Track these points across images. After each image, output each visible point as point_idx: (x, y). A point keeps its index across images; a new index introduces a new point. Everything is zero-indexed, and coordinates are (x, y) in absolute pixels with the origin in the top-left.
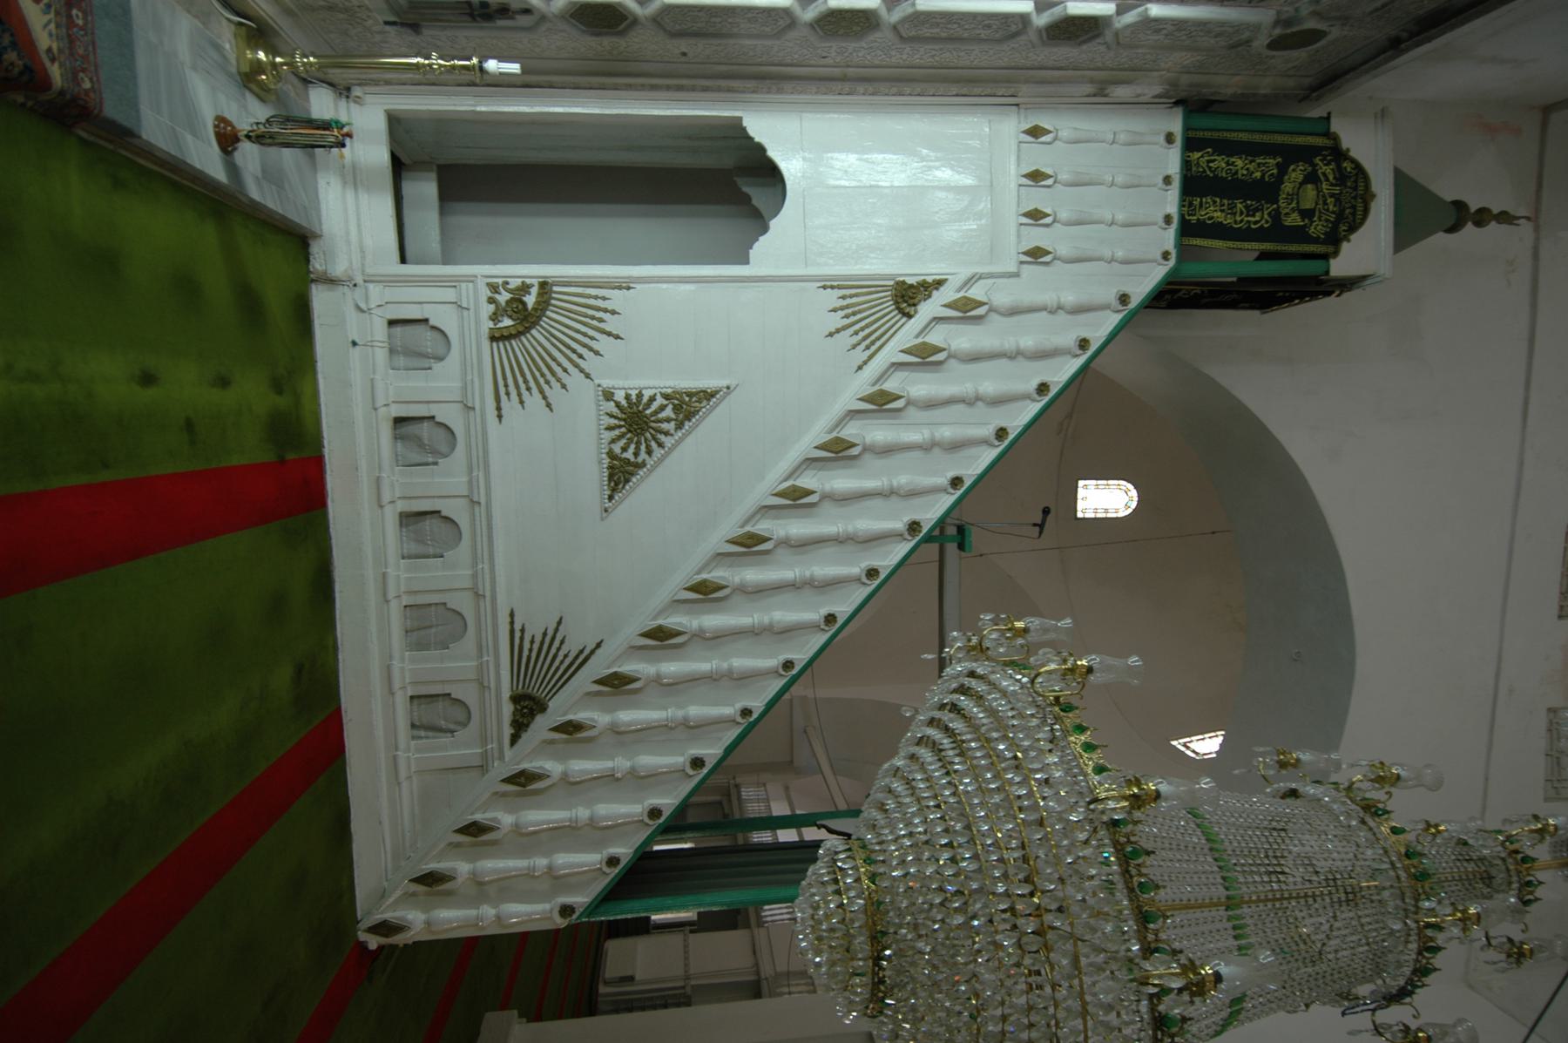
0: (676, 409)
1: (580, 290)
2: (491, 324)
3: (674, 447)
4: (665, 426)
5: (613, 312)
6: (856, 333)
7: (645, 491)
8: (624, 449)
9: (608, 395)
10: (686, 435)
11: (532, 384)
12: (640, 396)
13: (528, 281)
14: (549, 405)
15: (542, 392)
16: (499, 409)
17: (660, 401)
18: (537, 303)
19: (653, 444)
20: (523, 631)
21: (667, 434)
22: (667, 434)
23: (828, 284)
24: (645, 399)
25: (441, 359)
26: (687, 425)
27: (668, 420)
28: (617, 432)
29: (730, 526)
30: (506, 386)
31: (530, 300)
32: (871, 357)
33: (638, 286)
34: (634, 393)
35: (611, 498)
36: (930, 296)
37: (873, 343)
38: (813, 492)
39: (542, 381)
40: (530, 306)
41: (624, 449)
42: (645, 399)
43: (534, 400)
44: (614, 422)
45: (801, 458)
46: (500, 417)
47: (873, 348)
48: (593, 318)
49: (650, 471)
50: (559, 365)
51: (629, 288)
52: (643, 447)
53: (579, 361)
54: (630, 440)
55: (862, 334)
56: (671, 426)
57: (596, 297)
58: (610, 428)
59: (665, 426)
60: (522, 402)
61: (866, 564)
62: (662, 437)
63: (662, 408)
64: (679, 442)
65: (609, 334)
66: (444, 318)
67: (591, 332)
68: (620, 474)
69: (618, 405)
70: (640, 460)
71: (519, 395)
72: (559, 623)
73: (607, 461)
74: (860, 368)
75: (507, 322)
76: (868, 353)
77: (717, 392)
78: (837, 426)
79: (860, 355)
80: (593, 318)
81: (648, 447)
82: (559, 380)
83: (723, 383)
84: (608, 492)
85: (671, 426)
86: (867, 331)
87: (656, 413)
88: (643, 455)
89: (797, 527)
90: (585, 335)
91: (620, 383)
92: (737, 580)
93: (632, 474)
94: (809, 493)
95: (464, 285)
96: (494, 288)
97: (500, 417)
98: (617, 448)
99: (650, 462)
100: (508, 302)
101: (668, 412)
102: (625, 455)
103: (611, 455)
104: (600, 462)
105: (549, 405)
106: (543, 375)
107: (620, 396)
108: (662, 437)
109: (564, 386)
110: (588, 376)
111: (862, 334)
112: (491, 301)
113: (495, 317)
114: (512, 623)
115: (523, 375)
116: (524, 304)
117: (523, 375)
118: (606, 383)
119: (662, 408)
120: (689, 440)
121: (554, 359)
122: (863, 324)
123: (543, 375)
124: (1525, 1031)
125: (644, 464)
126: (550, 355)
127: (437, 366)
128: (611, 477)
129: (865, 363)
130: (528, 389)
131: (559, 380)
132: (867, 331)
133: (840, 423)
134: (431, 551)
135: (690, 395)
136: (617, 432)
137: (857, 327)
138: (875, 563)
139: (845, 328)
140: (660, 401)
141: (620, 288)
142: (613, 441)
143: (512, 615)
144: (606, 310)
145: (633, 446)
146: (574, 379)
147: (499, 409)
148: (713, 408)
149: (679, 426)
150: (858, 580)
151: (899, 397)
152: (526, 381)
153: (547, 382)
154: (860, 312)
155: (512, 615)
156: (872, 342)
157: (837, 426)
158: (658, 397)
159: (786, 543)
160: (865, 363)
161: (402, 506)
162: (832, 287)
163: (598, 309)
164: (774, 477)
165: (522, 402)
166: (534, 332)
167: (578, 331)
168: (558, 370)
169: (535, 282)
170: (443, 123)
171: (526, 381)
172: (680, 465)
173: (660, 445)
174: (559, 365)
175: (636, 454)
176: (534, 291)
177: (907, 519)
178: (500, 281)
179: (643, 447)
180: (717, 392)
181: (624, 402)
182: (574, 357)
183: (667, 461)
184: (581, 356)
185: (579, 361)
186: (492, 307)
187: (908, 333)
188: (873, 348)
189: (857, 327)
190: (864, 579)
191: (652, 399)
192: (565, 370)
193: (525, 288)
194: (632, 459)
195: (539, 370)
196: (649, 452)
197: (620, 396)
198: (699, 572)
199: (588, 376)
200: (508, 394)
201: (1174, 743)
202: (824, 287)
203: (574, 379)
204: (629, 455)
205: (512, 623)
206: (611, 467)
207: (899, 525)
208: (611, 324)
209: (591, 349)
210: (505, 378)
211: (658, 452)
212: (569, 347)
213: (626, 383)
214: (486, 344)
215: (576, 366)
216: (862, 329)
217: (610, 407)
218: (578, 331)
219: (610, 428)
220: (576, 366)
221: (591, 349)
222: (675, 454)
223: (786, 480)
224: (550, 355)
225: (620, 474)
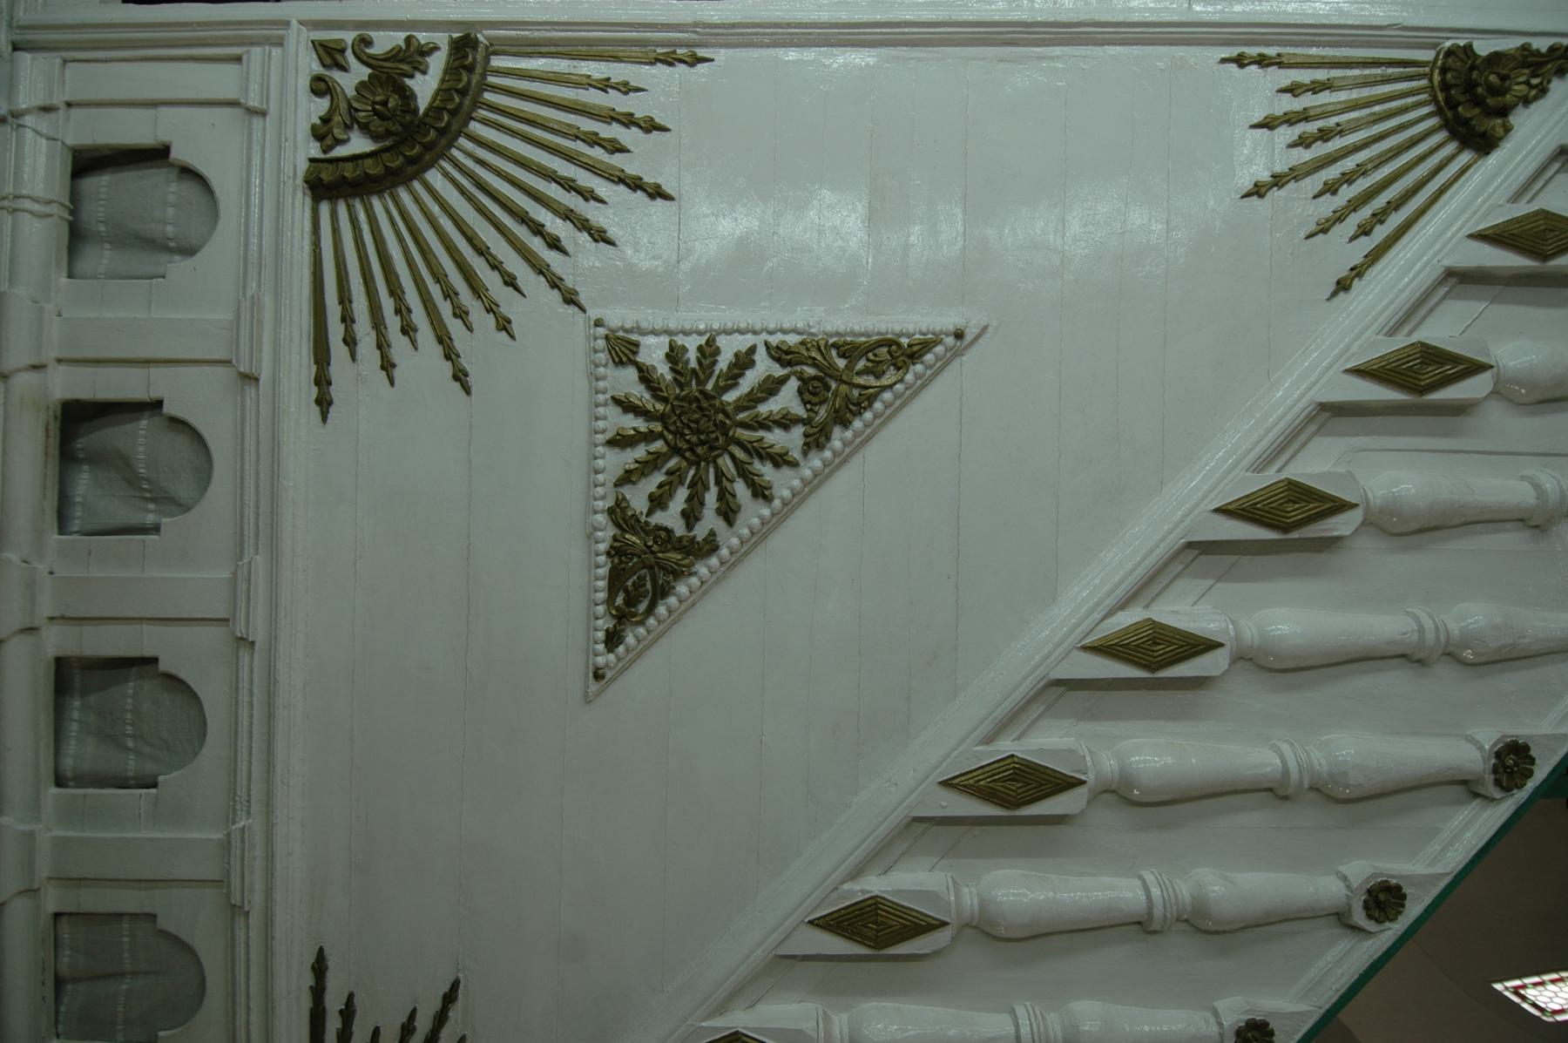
0: (811, 392)
1: (561, 65)
2: (315, 150)
3: (799, 498)
4: (776, 438)
5: (651, 126)
6: (1331, 188)
7: (710, 622)
8: (658, 501)
9: (623, 350)
10: (830, 470)
11: (419, 317)
12: (709, 352)
13: (423, 37)
14: (460, 376)
15: (443, 338)
16: (322, 381)
17: (764, 367)
18: (444, 92)
19: (741, 489)
20: (348, 1014)
21: (780, 460)
22: (780, 460)
23: (1252, 47)
24: (724, 361)
25: (189, 251)
26: (838, 437)
27: (786, 422)
28: (640, 452)
29: (953, 737)
30: (347, 319)
31: (425, 87)
32: (1374, 256)
33: (721, 55)
34: (692, 344)
35: (613, 639)
36: (1543, 91)
37: (1379, 217)
38: (1211, 646)
39: (445, 308)
40: (423, 103)
41: (658, 501)
42: (724, 361)
43: (421, 362)
44: (632, 423)
45: (1176, 539)
46: (324, 403)
47: (1381, 233)
48: (593, 140)
49: (729, 566)
50: (495, 265)
51: (697, 60)
52: (711, 498)
53: (550, 256)
54: (675, 477)
55: (1347, 193)
56: (790, 440)
57: (605, 85)
58: (620, 441)
59: (776, 438)
60: (387, 366)
61: (1362, 869)
62: (766, 471)
63: (771, 387)
64: (820, 479)
65: (635, 184)
66: (198, 140)
67: (585, 179)
68: (643, 573)
69: (646, 376)
70: (700, 532)
71: (382, 345)
72: (450, 998)
73: (607, 533)
74: (1343, 286)
75: (359, 144)
76: (1366, 244)
77: (927, 346)
78: (1281, 449)
79: (1342, 250)
80: (593, 140)
81: (725, 496)
82: (491, 308)
83: (945, 320)
84: (605, 623)
85: (790, 440)
86: (1362, 184)
87: (753, 399)
88: (710, 520)
89: (1151, 748)
90: (569, 185)
91: (649, 317)
92: (969, 898)
93: (678, 573)
94: (1198, 646)
95: (256, 51)
96: (330, 54)
97: (324, 403)
98: (638, 498)
99: (729, 540)
100: (361, 86)
101: (787, 400)
102: (659, 518)
103: (619, 514)
104: (590, 536)
105: (460, 376)
106: (450, 294)
107: (653, 352)
108: (766, 471)
109: (504, 325)
110: (570, 299)
111: (1347, 193)
112: (320, 86)
113: (322, 132)
114: (318, 991)
115: (395, 291)
116: (407, 96)
117: (395, 291)
118: (619, 316)
119: (771, 387)
120: (842, 481)
121: (482, 251)
122: (1349, 164)
123: (450, 294)
124: (163, 110)
125: (710, 546)
126: (471, 239)
127: (179, 268)
128: (616, 579)
129: (1358, 272)
130: (408, 330)
131: (491, 308)
132: (1362, 184)
133: (1290, 442)
134: (131, 765)
135: (849, 350)
136: (640, 452)
137: (1333, 172)
138: (1396, 867)
139: (1295, 174)
140: (764, 367)
141: (669, 60)
142: (627, 478)
143: (320, 967)
144: (628, 121)
145: (682, 494)
146: (534, 304)
147: (322, 381)
148: (916, 391)
149: (816, 440)
150: (1341, 918)
151: (1475, 368)
152: (402, 310)
153: (461, 314)
154: (1340, 131)
155: (320, 967)
156: (1381, 217)
157: (1281, 449)
158: (761, 356)
159: (1123, 795)
160: (1358, 272)
161: (57, 641)
162: (1262, 61)
163: (612, 117)
164: (1084, 599)
165: (387, 366)
166: (434, 177)
167: (551, 176)
168: (491, 280)
169: (442, 39)
170: (497, 38)
171: (402, 310)
172: (815, 556)
173: (761, 492)
174: (495, 265)
175: (691, 516)
176: (437, 63)
177: (1489, 736)
178: (349, 37)
179: (711, 498)
180: (927, 346)
181: (663, 370)
182: (536, 244)
183: (777, 541)
184: (554, 244)
185: (550, 256)
186: (324, 104)
187: (1487, 188)
188: (1381, 233)
189: (1333, 172)
190: (1359, 918)
191: (744, 362)
192: (510, 282)
193: (412, 56)
194: (679, 529)
195: (440, 277)
196: (728, 513)
197: (653, 352)
198: (856, 873)
199: (570, 299)
200: (350, 341)
201: (1498, 987)
202: (1240, 61)
203: (534, 304)
204: (671, 518)
205: (318, 991)
206: (617, 551)
207: (1468, 751)
208: (642, 154)
209: (583, 225)
210: (345, 299)
211: (752, 512)
212: (523, 219)
213: (666, 322)
214: (299, 204)
215: (541, 269)
216: (1348, 178)
217: (626, 381)
218: (551, 176)
219: (620, 441)
220: (541, 269)
221: (583, 225)
222: (802, 520)
223: (1123, 605)
224: (471, 239)
225: (643, 573)
